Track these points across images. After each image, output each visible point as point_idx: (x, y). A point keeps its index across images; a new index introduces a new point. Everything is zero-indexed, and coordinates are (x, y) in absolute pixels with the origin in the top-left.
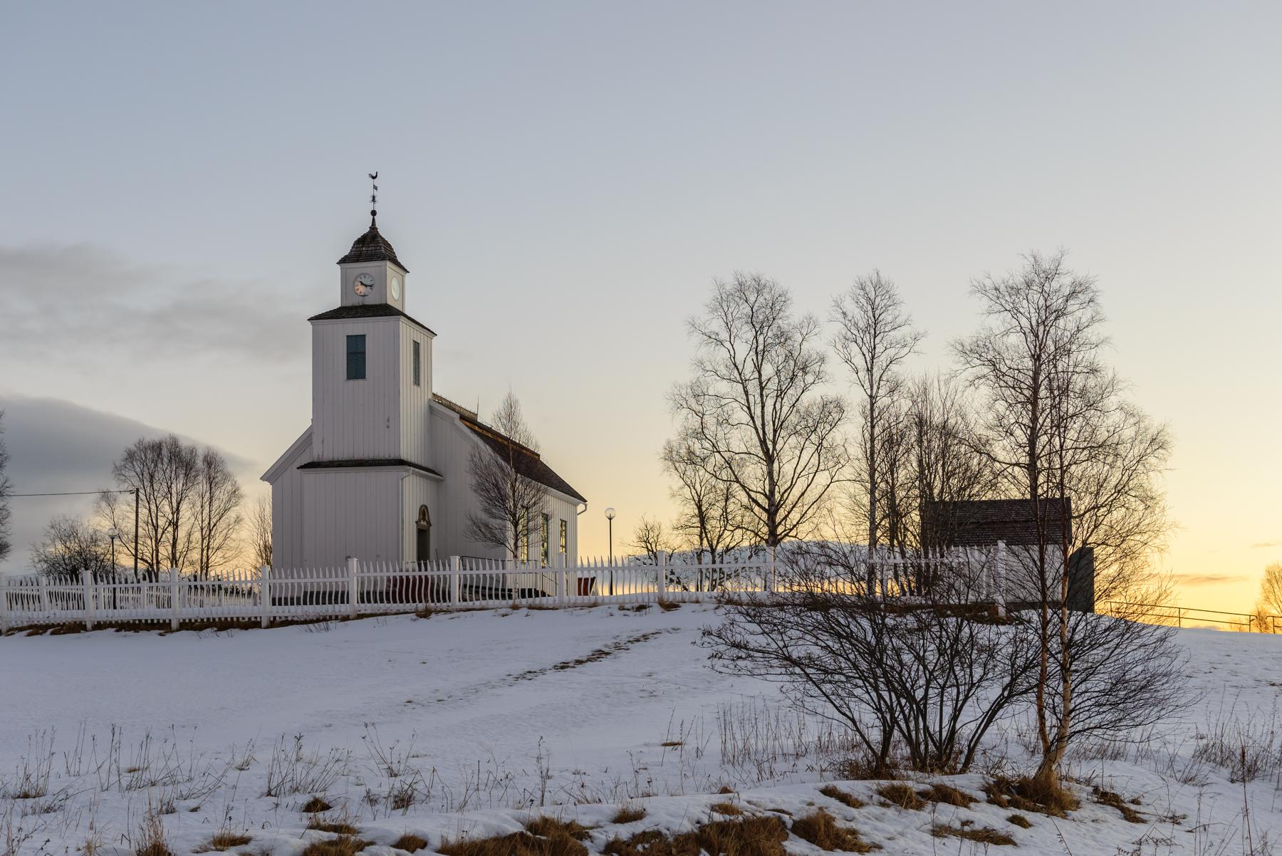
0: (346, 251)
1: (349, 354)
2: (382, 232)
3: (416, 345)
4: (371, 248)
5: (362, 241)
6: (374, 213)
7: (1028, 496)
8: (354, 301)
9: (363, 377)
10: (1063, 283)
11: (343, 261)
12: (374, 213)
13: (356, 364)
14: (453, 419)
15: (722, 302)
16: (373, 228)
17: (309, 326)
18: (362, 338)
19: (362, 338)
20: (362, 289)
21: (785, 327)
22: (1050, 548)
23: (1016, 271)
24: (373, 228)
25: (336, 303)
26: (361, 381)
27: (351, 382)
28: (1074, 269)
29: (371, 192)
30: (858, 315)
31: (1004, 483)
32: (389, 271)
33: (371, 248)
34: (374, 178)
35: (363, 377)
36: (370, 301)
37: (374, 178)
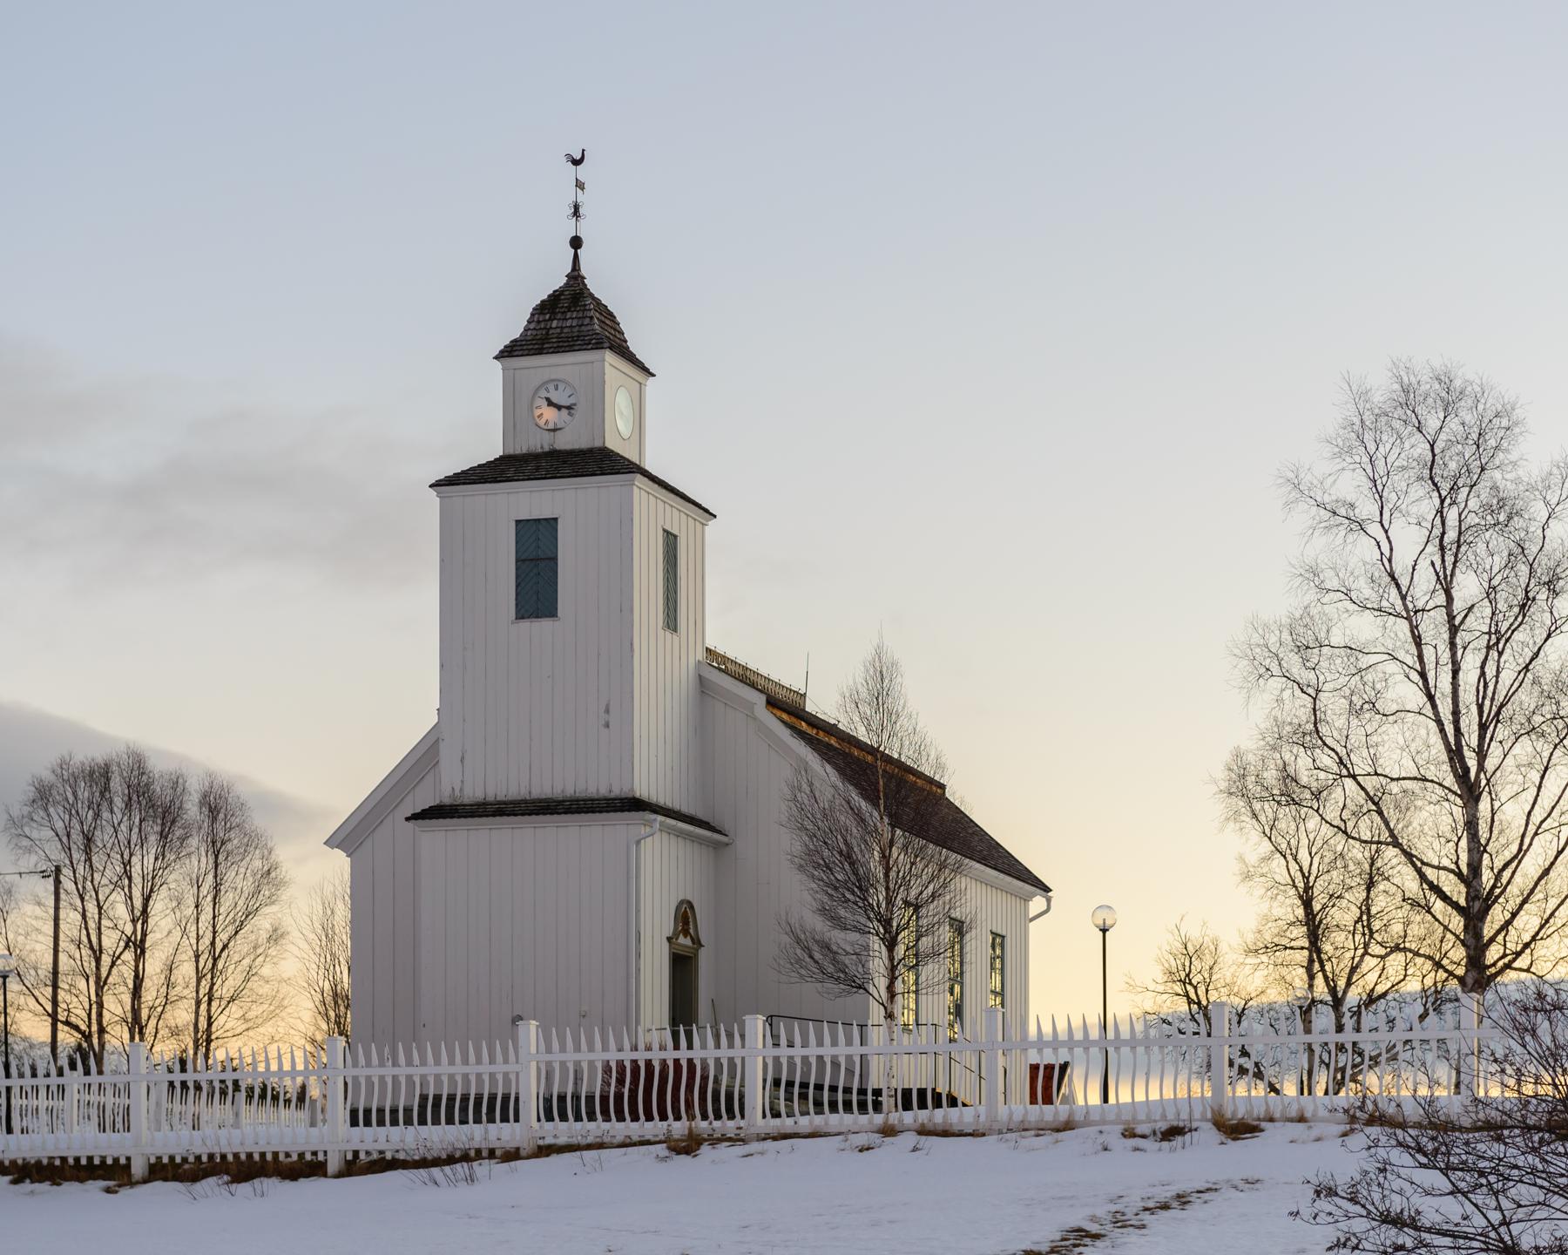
0: (515, 328)
3: (671, 540)
4: (570, 322)
5: (550, 307)
6: (576, 243)
8: (536, 442)
11: (509, 352)
12: (576, 243)
13: (536, 588)
16: (575, 276)
20: (550, 414)
24: (575, 276)
25: (491, 449)
26: (545, 625)
27: (525, 625)
29: (570, 194)
33: (570, 322)
34: (576, 162)
36: (564, 442)
37: (576, 162)
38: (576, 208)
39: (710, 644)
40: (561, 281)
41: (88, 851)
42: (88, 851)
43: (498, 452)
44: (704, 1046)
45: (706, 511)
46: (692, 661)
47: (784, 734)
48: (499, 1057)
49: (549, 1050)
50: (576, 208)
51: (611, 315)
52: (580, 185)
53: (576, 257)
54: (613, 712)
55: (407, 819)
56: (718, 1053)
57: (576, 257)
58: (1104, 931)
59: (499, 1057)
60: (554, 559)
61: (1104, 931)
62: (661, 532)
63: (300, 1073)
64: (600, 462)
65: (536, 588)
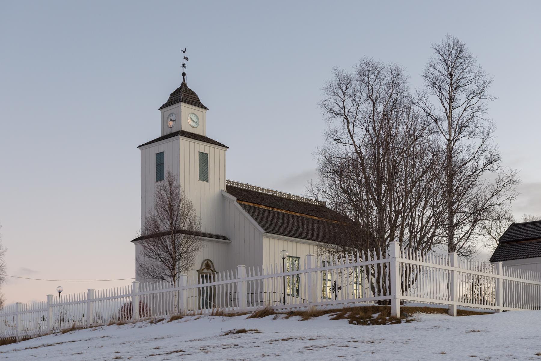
0: (165, 100)
1: (157, 165)
2: (190, 86)
3: (204, 158)
4: (184, 95)
5: (173, 94)
6: (184, 74)
12: (184, 74)
16: (184, 85)
17: (139, 151)
24: (184, 85)
25: (159, 135)
29: (182, 61)
33: (184, 95)
34: (184, 52)
36: (174, 130)
39: (229, 178)
40: (179, 86)
41: (119, 318)
42: (119, 318)
46: (94, 311)
49: (248, 276)
51: (194, 94)
52: (184, 65)
53: (184, 78)
55: (133, 241)
57: (184, 78)
58: (60, 293)
60: (164, 163)
61: (60, 293)
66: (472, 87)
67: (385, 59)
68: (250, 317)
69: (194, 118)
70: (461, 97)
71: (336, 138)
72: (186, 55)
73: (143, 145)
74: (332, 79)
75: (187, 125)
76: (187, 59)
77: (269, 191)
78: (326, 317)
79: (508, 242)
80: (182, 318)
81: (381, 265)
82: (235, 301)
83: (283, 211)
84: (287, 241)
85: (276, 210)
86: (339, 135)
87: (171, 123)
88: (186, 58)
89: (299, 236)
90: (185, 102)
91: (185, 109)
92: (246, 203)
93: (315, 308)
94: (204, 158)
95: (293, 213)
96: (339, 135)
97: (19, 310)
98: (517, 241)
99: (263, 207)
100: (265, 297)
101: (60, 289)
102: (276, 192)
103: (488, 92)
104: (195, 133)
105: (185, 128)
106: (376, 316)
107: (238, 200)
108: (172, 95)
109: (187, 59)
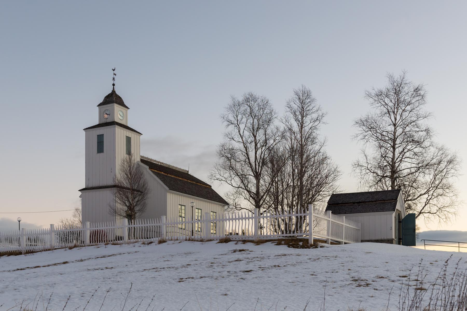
0: (101, 101)
1: (98, 143)
2: (117, 93)
3: (129, 140)
4: (113, 99)
5: (107, 97)
6: (114, 85)
7: (390, 189)
8: (103, 121)
9: (103, 152)
10: (407, 90)
11: (99, 105)
12: (114, 85)
13: (100, 149)
14: (146, 169)
15: (235, 107)
16: (113, 92)
17: (84, 132)
18: (102, 135)
19: (102, 135)
20: (106, 116)
21: (371, 177)
22: (390, 189)
23: (384, 85)
24: (113, 92)
25: (97, 123)
26: (102, 154)
27: (98, 154)
28: (413, 80)
29: (113, 76)
30: (296, 106)
31: (321, 232)
32: (115, 106)
33: (113, 99)
34: (114, 70)
35: (103, 152)
36: (109, 121)
37: (114, 70)
38: (114, 78)
39: (142, 154)
40: (110, 92)
43: (98, 123)
44: (137, 224)
45: (139, 133)
47: (152, 173)
48: (146, 223)
50: (114, 78)
51: (120, 98)
54: (113, 169)
55: (80, 190)
56: (140, 225)
59: (146, 223)
60: (103, 142)
62: (125, 137)
63: (262, 217)
64: (113, 123)
65: (100, 149)
66: (314, 116)
67: (259, 93)
68: (219, 243)
69: (121, 114)
70: (307, 120)
71: (230, 137)
72: (115, 72)
73: (87, 129)
74: (229, 102)
75: (118, 118)
76: (115, 75)
77: (159, 162)
78: (269, 243)
79: (333, 204)
80: (166, 242)
81: (299, 217)
82: (159, 234)
83: (173, 176)
84: (179, 195)
85: (169, 175)
86: (233, 135)
87: (106, 116)
88: (115, 74)
89: (185, 193)
90: (116, 103)
91: (117, 107)
92: (156, 171)
93: (260, 239)
94: (129, 140)
95: (178, 178)
96: (233, 135)
97: (24, 233)
98: (338, 204)
99: (163, 173)
100: (164, 231)
101: (19, 219)
102: (162, 163)
103: (324, 120)
104: (122, 123)
105: (116, 120)
106: (301, 243)
107: (150, 168)
108: (106, 97)
109: (115, 75)
